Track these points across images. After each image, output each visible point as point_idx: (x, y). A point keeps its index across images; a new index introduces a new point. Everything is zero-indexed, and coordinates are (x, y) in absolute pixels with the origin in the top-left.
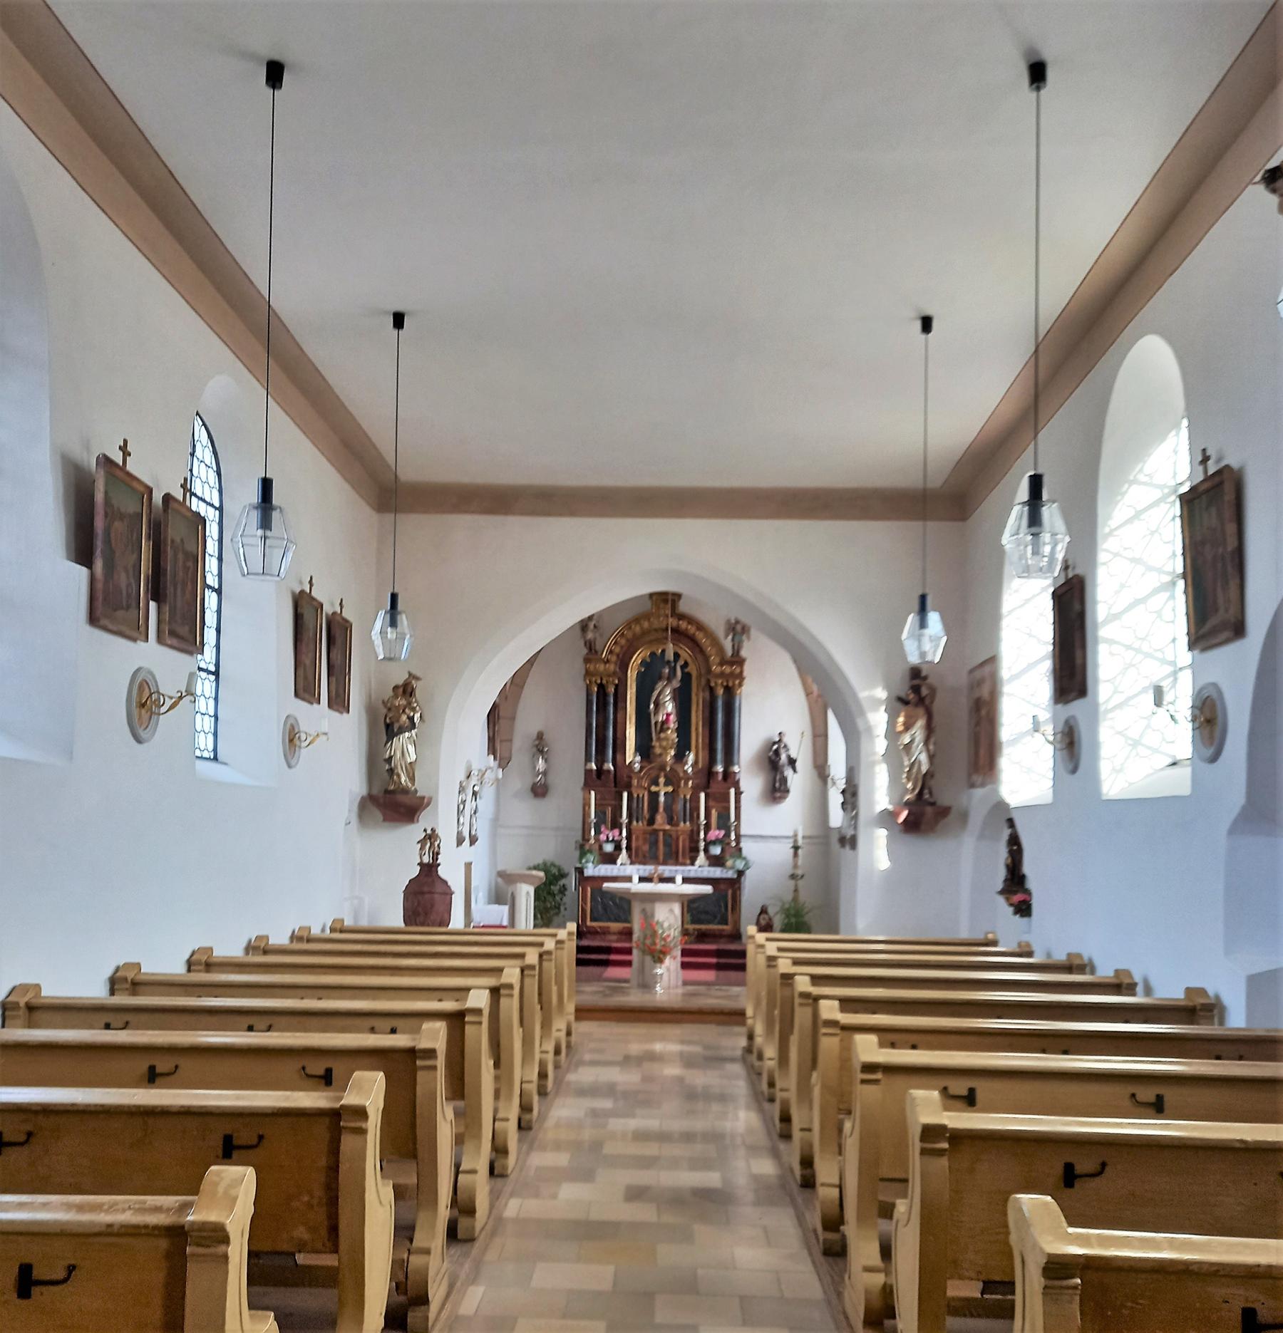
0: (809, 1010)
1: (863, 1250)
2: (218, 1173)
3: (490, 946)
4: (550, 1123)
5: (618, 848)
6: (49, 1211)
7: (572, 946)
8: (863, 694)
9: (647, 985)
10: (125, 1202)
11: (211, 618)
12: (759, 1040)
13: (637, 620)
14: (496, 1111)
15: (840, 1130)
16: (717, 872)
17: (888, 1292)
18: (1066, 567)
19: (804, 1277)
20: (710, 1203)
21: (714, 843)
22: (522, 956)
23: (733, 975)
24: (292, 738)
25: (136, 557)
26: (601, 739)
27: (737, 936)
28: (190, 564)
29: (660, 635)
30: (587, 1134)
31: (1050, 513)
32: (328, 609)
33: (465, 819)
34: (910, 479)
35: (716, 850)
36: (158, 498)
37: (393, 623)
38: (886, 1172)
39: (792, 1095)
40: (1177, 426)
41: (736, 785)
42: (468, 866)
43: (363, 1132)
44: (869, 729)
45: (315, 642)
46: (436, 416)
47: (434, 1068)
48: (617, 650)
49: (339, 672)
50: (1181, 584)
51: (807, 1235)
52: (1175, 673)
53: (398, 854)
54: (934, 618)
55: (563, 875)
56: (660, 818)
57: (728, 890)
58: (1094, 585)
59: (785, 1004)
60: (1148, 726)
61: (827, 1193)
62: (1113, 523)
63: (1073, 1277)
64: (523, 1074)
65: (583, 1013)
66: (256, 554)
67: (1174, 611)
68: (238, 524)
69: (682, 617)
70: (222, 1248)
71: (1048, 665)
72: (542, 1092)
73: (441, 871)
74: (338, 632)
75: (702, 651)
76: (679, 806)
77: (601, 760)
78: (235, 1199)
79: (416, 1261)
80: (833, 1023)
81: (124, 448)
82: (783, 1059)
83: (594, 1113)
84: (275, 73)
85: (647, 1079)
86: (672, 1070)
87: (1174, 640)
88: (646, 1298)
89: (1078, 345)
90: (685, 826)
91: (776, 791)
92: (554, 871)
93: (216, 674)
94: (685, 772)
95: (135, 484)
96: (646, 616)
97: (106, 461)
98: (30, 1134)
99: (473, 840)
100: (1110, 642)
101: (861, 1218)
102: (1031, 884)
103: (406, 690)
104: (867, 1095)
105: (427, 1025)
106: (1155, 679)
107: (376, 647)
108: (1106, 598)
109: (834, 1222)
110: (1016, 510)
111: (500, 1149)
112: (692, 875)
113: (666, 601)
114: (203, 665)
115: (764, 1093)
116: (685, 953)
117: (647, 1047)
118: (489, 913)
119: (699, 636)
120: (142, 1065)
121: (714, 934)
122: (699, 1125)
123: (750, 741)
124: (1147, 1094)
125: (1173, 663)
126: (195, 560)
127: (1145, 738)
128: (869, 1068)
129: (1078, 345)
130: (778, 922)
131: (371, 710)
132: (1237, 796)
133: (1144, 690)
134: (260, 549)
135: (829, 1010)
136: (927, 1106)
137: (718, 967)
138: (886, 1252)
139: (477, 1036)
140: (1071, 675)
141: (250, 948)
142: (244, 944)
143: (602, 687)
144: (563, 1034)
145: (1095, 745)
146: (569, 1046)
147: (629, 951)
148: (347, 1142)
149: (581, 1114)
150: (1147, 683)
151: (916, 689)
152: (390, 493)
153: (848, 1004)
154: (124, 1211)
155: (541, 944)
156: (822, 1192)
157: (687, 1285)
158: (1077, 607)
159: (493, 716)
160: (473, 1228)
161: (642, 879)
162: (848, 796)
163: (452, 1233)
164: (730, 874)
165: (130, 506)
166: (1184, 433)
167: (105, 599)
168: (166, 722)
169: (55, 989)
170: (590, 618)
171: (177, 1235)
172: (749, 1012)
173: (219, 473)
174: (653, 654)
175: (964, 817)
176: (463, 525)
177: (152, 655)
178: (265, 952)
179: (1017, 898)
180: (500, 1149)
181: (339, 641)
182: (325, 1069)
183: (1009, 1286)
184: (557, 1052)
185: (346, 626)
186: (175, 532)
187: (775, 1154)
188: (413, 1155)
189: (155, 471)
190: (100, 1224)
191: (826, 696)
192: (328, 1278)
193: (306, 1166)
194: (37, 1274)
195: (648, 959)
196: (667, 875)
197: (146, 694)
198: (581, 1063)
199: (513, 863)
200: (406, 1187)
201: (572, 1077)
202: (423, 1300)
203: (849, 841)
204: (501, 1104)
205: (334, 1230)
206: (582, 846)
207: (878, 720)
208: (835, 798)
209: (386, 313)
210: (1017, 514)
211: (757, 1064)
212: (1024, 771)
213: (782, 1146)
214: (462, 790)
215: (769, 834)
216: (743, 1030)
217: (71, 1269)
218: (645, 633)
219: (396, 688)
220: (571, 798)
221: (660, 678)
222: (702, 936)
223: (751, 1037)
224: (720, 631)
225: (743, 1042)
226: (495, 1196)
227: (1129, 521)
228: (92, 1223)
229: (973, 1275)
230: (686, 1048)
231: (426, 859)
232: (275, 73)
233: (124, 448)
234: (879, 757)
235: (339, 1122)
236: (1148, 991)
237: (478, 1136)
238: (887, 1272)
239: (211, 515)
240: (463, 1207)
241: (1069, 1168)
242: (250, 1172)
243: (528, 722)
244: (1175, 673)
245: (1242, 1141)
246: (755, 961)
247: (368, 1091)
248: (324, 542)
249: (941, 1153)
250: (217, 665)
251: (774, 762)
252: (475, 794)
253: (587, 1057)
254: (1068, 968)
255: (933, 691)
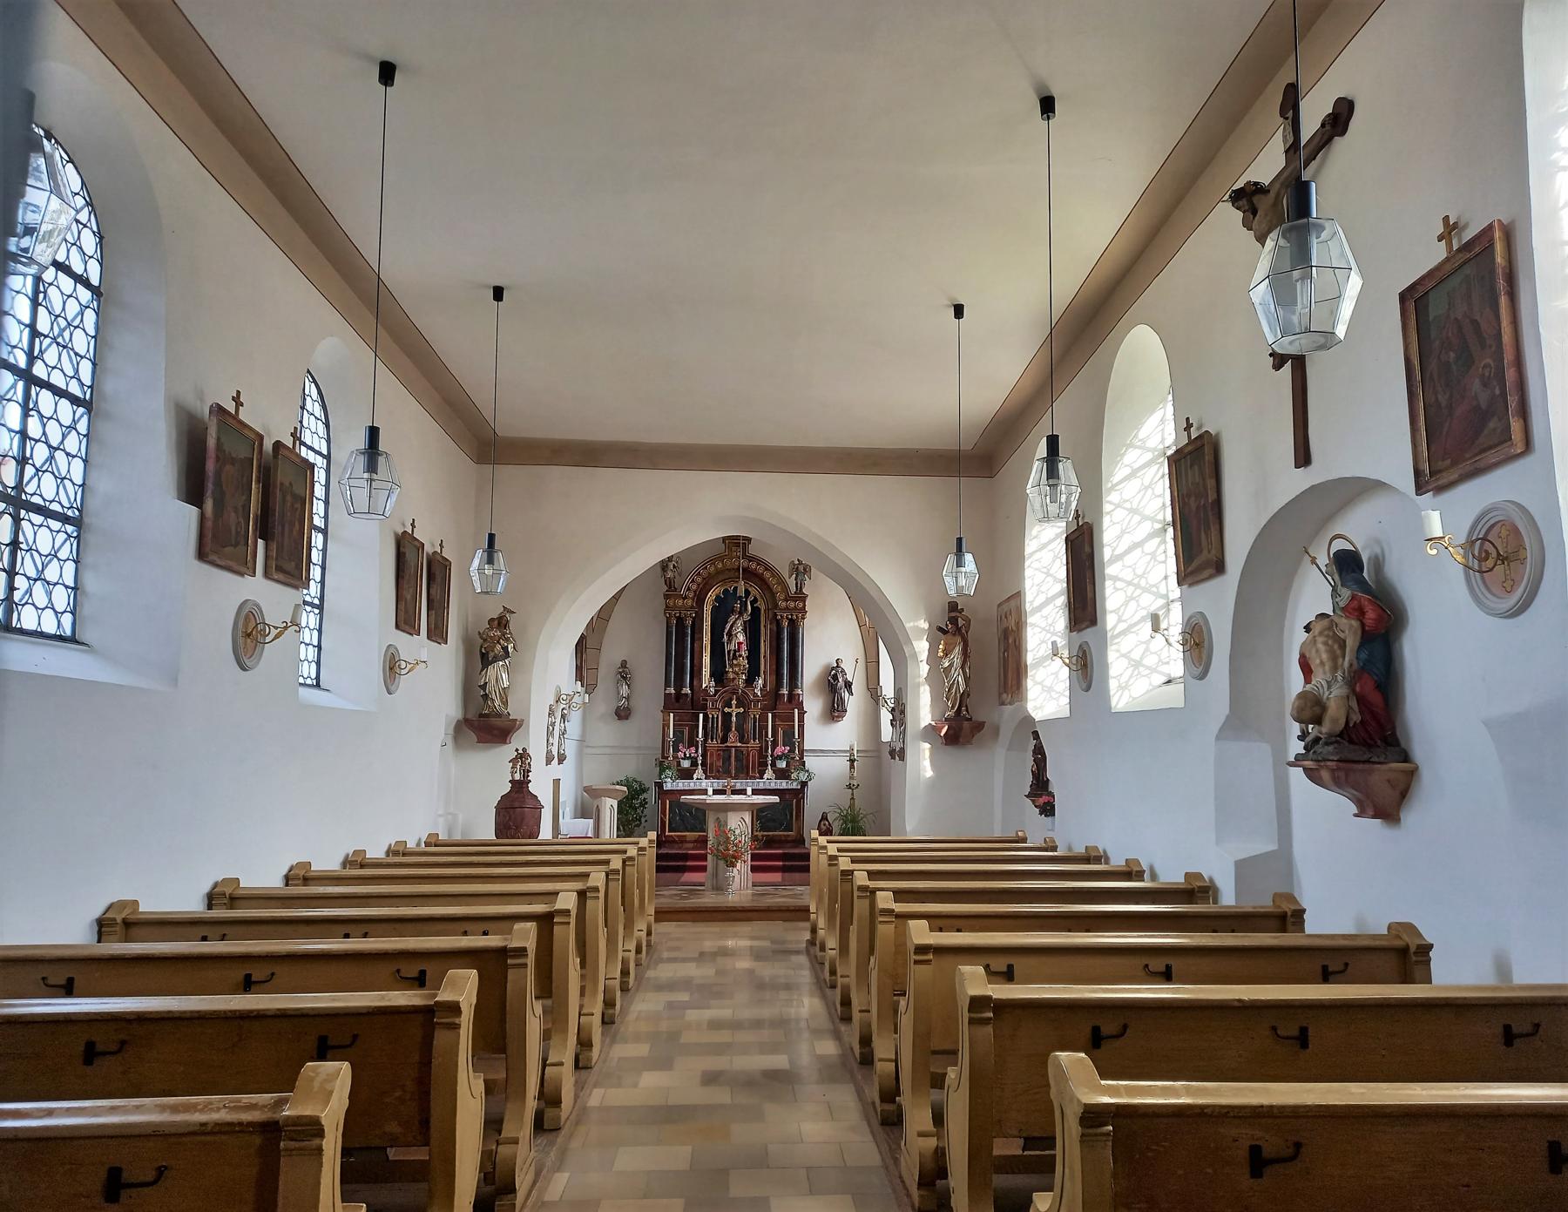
0: (867, 902)
1: (918, 1118)
2: (314, 1069)
3: (574, 858)
4: (631, 1017)
5: (694, 764)
6: (142, 1113)
7: (652, 853)
8: (908, 625)
9: (720, 888)
10: (220, 1101)
11: (316, 556)
12: (821, 933)
13: (712, 561)
14: (581, 1007)
15: (896, 1011)
16: (783, 784)
17: (940, 1154)
18: (1077, 517)
19: (864, 1147)
20: (778, 1082)
21: (780, 758)
22: (607, 862)
23: (797, 875)
24: (393, 667)
25: (245, 499)
26: (679, 660)
27: (800, 841)
28: (298, 505)
29: (732, 574)
30: (664, 1026)
31: (1065, 468)
32: (428, 549)
33: (555, 741)
34: (946, 443)
35: (782, 764)
36: (268, 445)
37: (490, 561)
38: (937, 1044)
39: (852, 981)
40: (1164, 400)
41: (800, 706)
42: (557, 782)
43: (457, 1027)
44: (915, 655)
45: (416, 578)
46: (527, 380)
47: (525, 965)
48: (694, 587)
49: (438, 607)
50: (1171, 530)
51: (866, 1106)
52: (1168, 604)
53: (490, 774)
54: (968, 558)
55: (644, 791)
56: (733, 736)
57: (793, 799)
58: (1101, 532)
59: (843, 894)
60: (1147, 650)
61: (884, 1068)
62: (1116, 479)
63: (1106, 1124)
64: (608, 972)
65: (662, 915)
66: (361, 496)
67: (1163, 558)
68: (345, 469)
69: (752, 559)
70: (316, 1141)
71: (1062, 600)
72: (625, 988)
73: (531, 787)
74: (438, 570)
75: (769, 589)
76: (750, 725)
77: (679, 684)
78: (331, 1092)
79: (504, 1150)
80: (890, 912)
81: (237, 400)
82: (844, 948)
83: (671, 1006)
84: (387, 73)
85: (719, 973)
86: (744, 964)
87: (1166, 578)
88: (720, 1175)
89: (1082, 332)
90: (754, 744)
91: (835, 711)
92: (636, 786)
93: (321, 607)
94: (755, 695)
95: (246, 432)
96: (721, 558)
97: (219, 410)
98: (123, 1043)
99: (562, 759)
100: (1115, 579)
101: (915, 1088)
102: (1054, 787)
103: (501, 623)
104: (919, 975)
105: (518, 926)
106: (1152, 609)
107: (474, 583)
108: (1112, 537)
109: (890, 1094)
110: (1036, 465)
111: (585, 1043)
112: (761, 786)
113: (738, 545)
114: (308, 599)
115: (827, 981)
116: (754, 857)
117: (721, 943)
118: (574, 826)
119: (767, 575)
120: (238, 974)
121: (781, 839)
122: (766, 1013)
123: (812, 666)
124: (1158, 964)
125: (1167, 596)
126: (303, 502)
127: (1144, 663)
128: (922, 949)
129: (1082, 332)
130: (836, 827)
131: (467, 642)
132: (1220, 706)
133: (1143, 619)
134: (366, 492)
135: (885, 900)
136: (974, 981)
137: (784, 869)
138: (938, 1118)
139: (566, 935)
140: (1083, 604)
141: (346, 863)
142: (341, 859)
143: (680, 620)
144: (644, 934)
145: (1105, 666)
146: (649, 945)
147: (704, 858)
148: (440, 1038)
149: (661, 1008)
150: (1144, 613)
151: (953, 621)
152: (487, 446)
153: (900, 895)
154: (219, 1109)
155: (625, 852)
156: (879, 1066)
157: (759, 1161)
158: (1087, 549)
159: (581, 646)
160: (559, 1118)
161: (716, 792)
162: (897, 713)
163: (539, 1125)
164: (795, 785)
165: (241, 452)
166: (1170, 408)
167: (214, 536)
168: (271, 651)
169: (153, 903)
170: (670, 559)
171: (271, 1130)
172: (813, 909)
173: (327, 425)
174: (726, 591)
175: (996, 731)
176: (556, 475)
177: (258, 589)
178: (362, 866)
179: (1041, 801)
180: (585, 1043)
181: (438, 579)
182: (419, 970)
183: (1050, 1142)
184: (639, 951)
185: (446, 565)
186: (283, 475)
187: (837, 1036)
188: (502, 1049)
189: (267, 418)
190: (195, 1124)
191: (877, 627)
192: (419, 1172)
193: (399, 1064)
194: (126, 1176)
195: (722, 863)
196: (738, 787)
197: (252, 624)
198: (661, 961)
199: (596, 780)
200: (494, 1081)
201: (650, 974)
202: (510, 1189)
203: (898, 753)
204: (586, 1000)
205: (425, 1123)
206: (661, 763)
207: (922, 647)
208: (886, 717)
209: (487, 287)
210: (1037, 469)
211: (820, 954)
212: (1046, 692)
213: (843, 1028)
214: (551, 713)
215: (829, 746)
216: (807, 925)
217: (161, 1172)
218: (718, 572)
219: (492, 620)
220: (651, 718)
221: (733, 612)
222: (769, 843)
223: (814, 931)
224: (785, 572)
225: (808, 936)
226: (579, 1086)
227: (1127, 478)
228: (187, 1124)
229: (1015, 1133)
230: (756, 943)
231: (517, 777)
232: (387, 73)
233: (237, 400)
234: (922, 680)
235: (435, 1017)
236: (1154, 877)
237: (565, 1030)
238: (939, 1136)
239: (320, 462)
240: (549, 1098)
241: (1096, 1030)
242: (346, 1066)
243: (612, 653)
244: (1168, 604)
245: (1239, 1000)
246: (818, 862)
247: (462, 988)
248: (424, 488)
249: (986, 1021)
250: (322, 599)
251: (833, 684)
252: (563, 716)
253: (665, 955)
254: (1086, 859)
255: (968, 621)
